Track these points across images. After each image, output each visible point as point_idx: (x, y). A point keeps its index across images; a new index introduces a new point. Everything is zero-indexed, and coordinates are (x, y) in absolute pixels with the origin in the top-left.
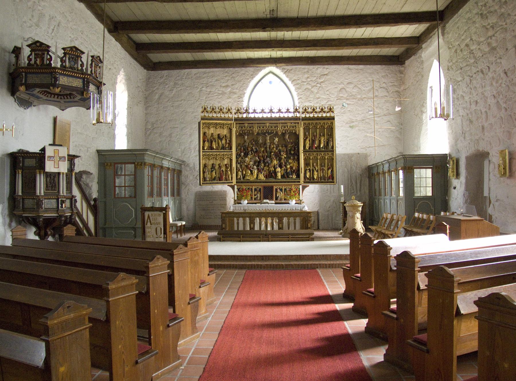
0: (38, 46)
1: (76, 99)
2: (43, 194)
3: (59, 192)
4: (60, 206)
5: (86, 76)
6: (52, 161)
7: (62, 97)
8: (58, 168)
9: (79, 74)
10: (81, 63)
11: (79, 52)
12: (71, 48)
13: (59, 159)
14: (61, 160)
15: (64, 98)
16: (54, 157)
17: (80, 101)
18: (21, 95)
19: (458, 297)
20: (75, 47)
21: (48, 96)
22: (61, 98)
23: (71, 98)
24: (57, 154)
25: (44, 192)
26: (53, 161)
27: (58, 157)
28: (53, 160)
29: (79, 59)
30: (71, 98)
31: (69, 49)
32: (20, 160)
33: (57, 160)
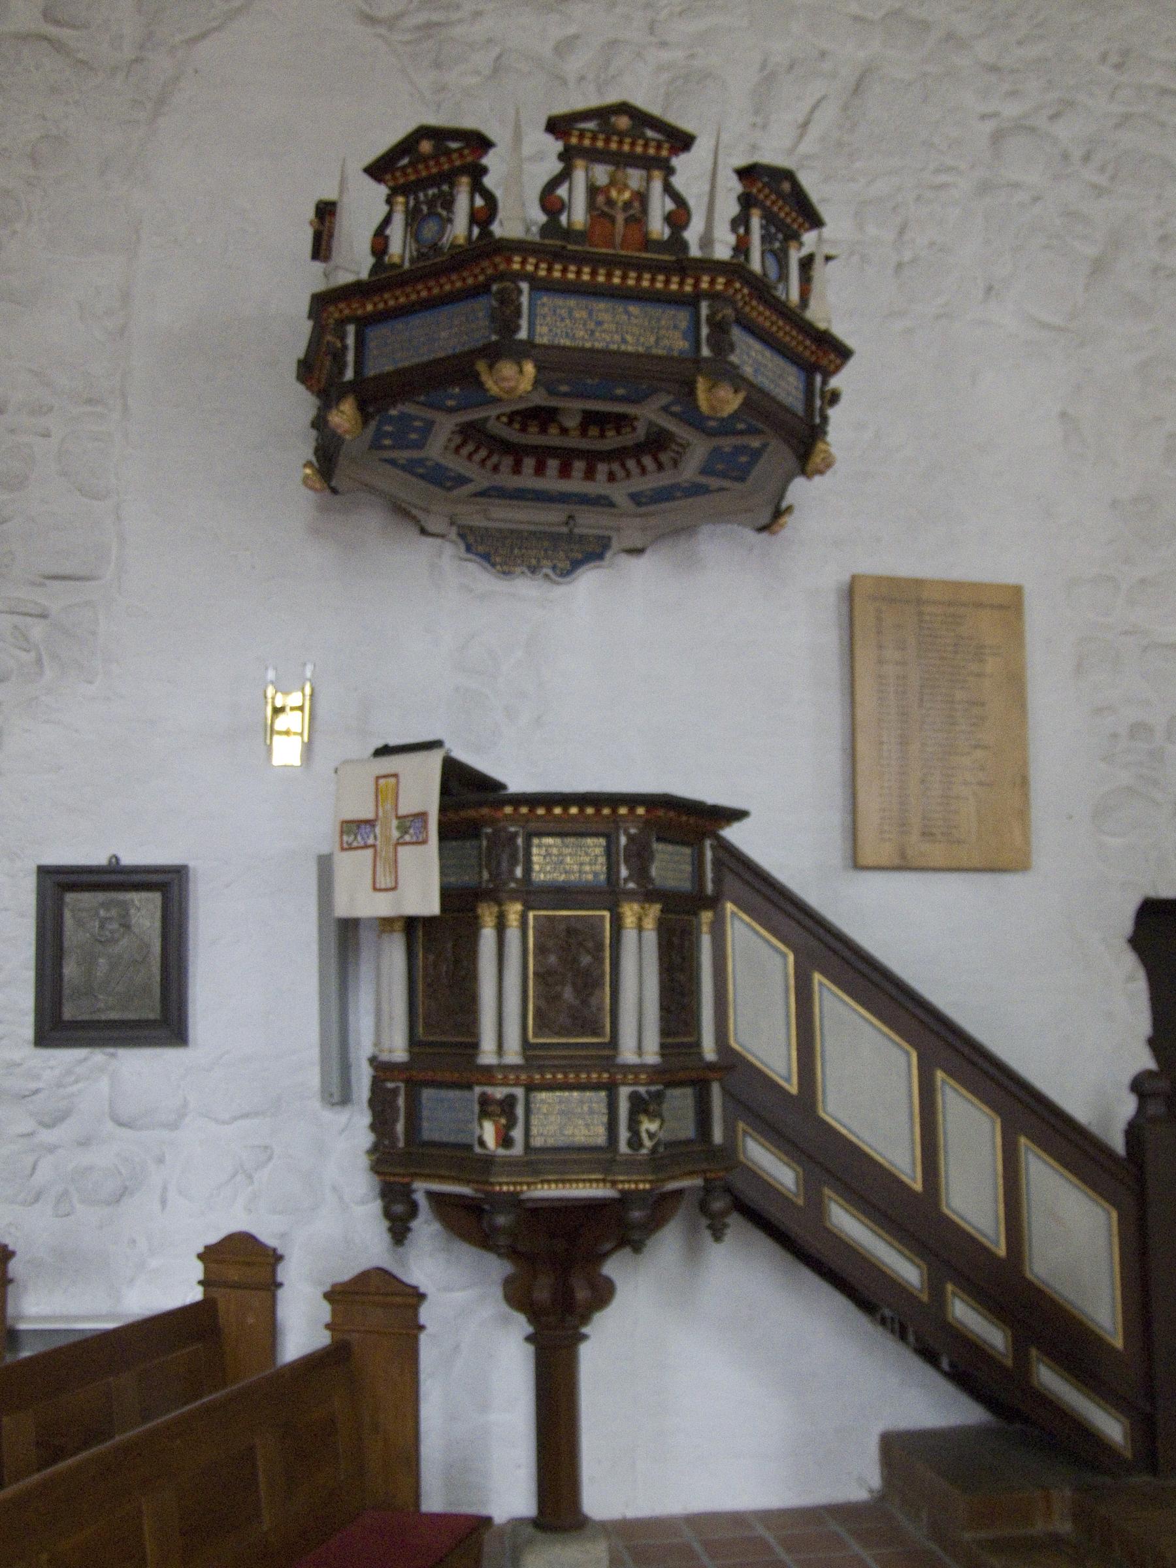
0: (425, 159)
1: (689, 470)
2: (513, 1056)
3: (614, 1043)
4: (624, 1134)
5: (706, 279)
6: (366, 847)
7: (616, 467)
8: (375, 889)
9: (656, 268)
10: (670, 205)
11: (650, 133)
12: (602, 114)
13: (395, 834)
14: (407, 838)
15: (628, 475)
16: (371, 823)
17: (714, 482)
18: (494, 516)
19: (545, 341)
20: (623, 108)
21: (502, 468)
22: (612, 477)
23: (660, 467)
24: (389, 806)
25: (526, 1044)
26: (369, 853)
27: (395, 823)
28: (371, 841)
29: (657, 186)
30: (660, 467)
31: (591, 125)
32: (629, 868)
33: (388, 838)
